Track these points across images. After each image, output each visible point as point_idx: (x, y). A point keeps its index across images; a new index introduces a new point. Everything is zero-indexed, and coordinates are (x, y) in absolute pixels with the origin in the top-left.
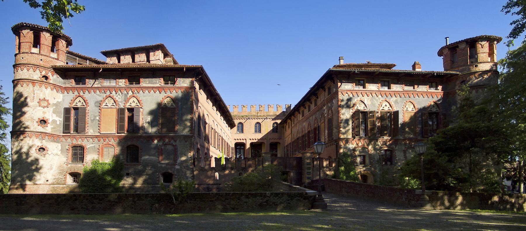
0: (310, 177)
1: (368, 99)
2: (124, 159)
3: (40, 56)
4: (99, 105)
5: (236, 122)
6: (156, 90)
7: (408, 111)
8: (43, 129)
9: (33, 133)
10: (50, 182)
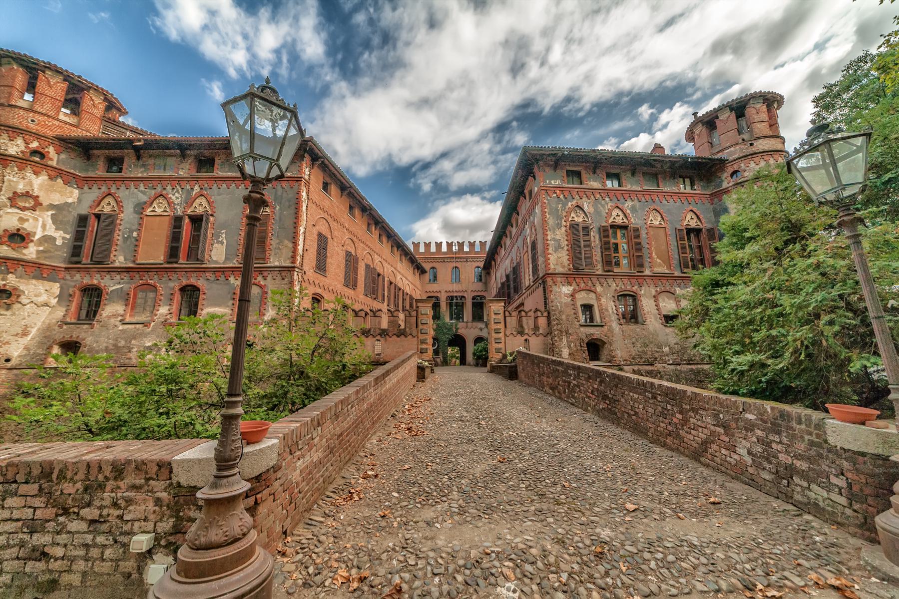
0: (501, 349)
3: (31, 115)
4: (141, 210)
5: (427, 266)
6: (240, 182)
7: (653, 225)
8: (14, 253)
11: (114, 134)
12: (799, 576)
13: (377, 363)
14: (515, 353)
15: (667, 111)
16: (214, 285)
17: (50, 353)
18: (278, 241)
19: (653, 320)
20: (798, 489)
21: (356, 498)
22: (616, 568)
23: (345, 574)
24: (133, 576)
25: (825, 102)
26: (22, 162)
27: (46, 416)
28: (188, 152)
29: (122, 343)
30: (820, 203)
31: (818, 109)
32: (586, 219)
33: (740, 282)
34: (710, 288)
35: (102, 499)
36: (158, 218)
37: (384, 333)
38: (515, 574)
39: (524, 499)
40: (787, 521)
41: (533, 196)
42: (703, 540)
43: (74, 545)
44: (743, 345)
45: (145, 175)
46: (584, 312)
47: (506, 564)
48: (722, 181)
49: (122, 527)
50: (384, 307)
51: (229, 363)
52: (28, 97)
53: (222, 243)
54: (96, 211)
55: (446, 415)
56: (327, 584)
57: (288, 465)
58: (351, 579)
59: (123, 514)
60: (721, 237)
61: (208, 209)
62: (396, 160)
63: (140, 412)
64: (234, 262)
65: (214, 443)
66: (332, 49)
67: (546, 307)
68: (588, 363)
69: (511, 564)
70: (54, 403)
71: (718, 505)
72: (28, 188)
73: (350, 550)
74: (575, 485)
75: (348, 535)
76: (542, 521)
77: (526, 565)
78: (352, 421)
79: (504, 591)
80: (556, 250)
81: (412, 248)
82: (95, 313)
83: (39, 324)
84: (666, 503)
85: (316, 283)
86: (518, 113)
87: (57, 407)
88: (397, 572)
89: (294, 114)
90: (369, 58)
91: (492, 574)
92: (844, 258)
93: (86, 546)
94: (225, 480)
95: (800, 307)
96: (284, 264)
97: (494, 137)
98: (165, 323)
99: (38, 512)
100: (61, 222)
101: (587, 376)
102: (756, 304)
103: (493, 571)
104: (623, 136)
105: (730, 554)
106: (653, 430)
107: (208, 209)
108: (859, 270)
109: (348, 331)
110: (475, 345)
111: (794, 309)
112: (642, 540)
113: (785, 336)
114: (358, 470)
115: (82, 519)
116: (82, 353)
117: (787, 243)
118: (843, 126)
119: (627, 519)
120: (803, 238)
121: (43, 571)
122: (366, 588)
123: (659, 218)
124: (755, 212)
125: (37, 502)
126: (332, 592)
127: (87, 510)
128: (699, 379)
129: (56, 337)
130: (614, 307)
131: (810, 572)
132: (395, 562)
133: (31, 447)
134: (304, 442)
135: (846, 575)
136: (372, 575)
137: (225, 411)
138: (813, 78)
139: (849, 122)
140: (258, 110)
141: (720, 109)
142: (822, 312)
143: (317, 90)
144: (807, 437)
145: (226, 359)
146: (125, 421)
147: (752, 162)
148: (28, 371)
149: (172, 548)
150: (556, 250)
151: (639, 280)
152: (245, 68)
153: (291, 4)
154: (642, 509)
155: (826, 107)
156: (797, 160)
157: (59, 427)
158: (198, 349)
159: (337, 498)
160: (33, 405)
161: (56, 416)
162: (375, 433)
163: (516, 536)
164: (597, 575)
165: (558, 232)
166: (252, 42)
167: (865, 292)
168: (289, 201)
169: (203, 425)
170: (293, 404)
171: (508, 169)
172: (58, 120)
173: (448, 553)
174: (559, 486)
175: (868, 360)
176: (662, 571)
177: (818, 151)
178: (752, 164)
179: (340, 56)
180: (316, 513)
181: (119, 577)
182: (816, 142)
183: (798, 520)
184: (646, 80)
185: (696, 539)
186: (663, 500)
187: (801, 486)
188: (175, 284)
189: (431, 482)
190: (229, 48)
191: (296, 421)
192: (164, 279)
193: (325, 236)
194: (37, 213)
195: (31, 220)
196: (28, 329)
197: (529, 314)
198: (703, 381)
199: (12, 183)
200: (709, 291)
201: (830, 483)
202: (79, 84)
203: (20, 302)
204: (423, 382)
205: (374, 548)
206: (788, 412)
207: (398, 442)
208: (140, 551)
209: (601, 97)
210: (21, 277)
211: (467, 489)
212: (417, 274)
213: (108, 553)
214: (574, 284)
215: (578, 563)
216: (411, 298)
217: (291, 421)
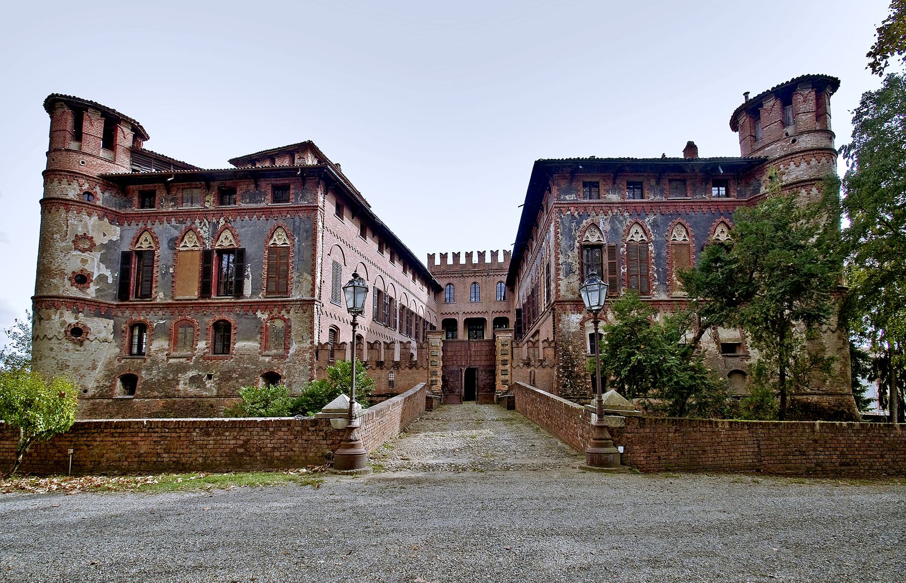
0: (507, 381)
1: (606, 220)
2: (207, 348)
5: (442, 283)
6: (261, 214)
9: (61, 300)
10: (90, 393)
32: (601, 239)
36: (190, 253)
48: (760, 185)
61: (233, 242)
80: (567, 275)
96: (305, 298)
123: (684, 233)
199: (74, 227)
202: (114, 117)
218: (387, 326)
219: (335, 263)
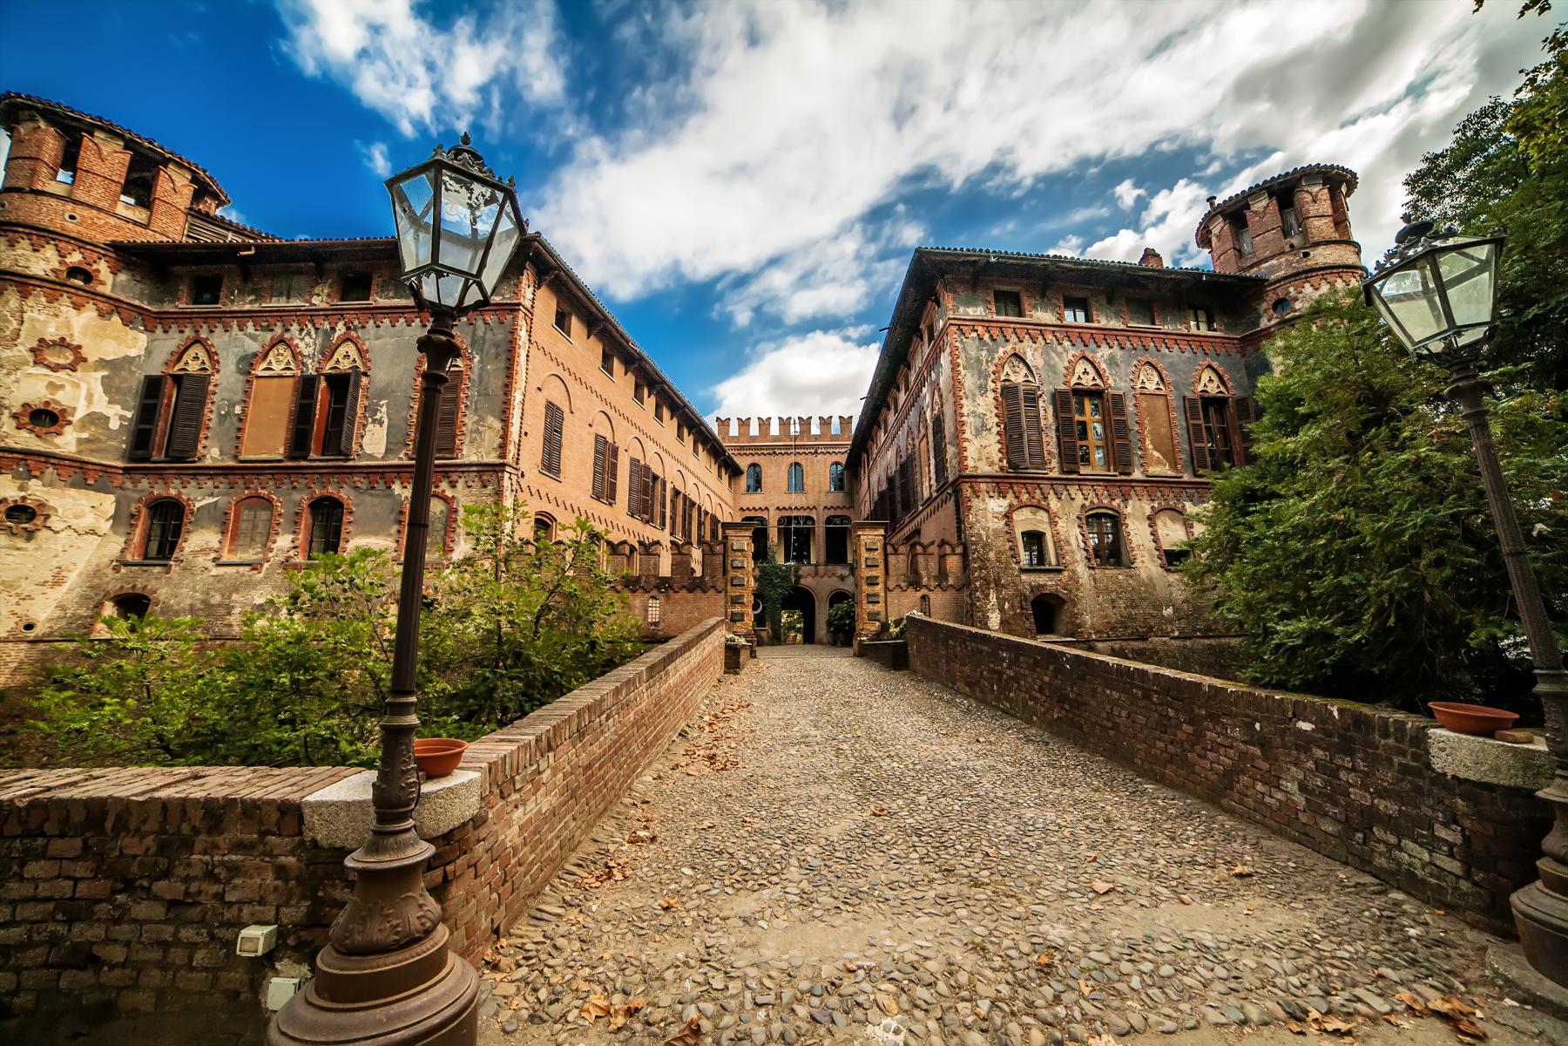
0: (878, 613)
3: (70, 206)
5: (743, 462)
6: (413, 316)
8: (41, 443)
11: (208, 236)
12: (1380, 995)
13: (653, 638)
14: (905, 622)
15: (1164, 192)
16: (368, 499)
17: (99, 614)
18: (476, 418)
19: (1146, 559)
20: (1382, 848)
21: (619, 876)
22: (1073, 989)
23: (603, 1003)
24: (243, 997)
25: (1426, 184)
26: (53, 287)
27: (93, 723)
28: (328, 266)
29: (217, 599)
30: (1420, 356)
31: (1415, 196)
32: (1030, 379)
33: (1291, 492)
34: (1242, 503)
35: (189, 865)
36: (276, 380)
37: (664, 585)
38: (898, 1003)
39: (916, 878)
40: (1361, 903)
41: (936, 334)
42: (1220, 937)
43: (143, 943)
44: (1292, 598)
45: (256, 307)
46: (1027, 547)
47: (885, 986)
48: (1260, 317)
49: (222, 914)
50: (665, 537)
51: (393, 636)
52: (63, 176)
53: (381, 423)
54: (175, 370)
55: (777, 733)
56: (570, 1017)
57: (499, 816)
58: (612, 1011)
59: (224, 891)
60: (1259, 414)
61: (359, 363)
62: (687, 270)
63: (247, 718)
64: (402, 455)
65: (372, 775)
66: (577, 83)
67: (959, 537)
68: (1034, 638)
69: (891, 987)
70: (107, 700)
71: (1248, 879)
72: (63, 333)
73: (610, 964)
74: (1007, 853)
75: (605, 938)
76: (947, 915)
77: (918, 988)
78: (609, 742)
79: (879, 1031)
80: (978, 433)
81: (714, 428)
82: (173, 546)
83: (81, 567)
84: (1161, 877)
85: (543, 494)
86: (907, 190)
87: (111, 706)
88: (692, 1002)
89: (510, 195)
90: (644, 97)
91: (859, 1005)
92: (1459, 453)
93: (164, 945)
94: (391, 840)
95: (1388, 536)
96: (486, 460)
97: (864, 231)
98: (286, 565)
99: (82, 886)
100: (118, 390)
101: (1031, 661)
102: (1316, 530)
103: (861, 999)
104: (1091, 233)
105: (1265, 960)
106: (1143, 753)
107: (359, 363)
108: (1484, 473)
109: (599, 581)
110: (831, 606)
111: (1379, 539)
112: (1118, 942)
113: (1364, 586)
114: (620, 828)
115: (156, 898)
116: (151, 614)
117: (1367, 425)
118: (1456, 225)
119: (1095, 906)
120: (1393, 417)
121: (90, 986)
122: (638, 1027)
123: (1156, 379)
124: (1314, 370)
125: (80, 870)
126: (579, 1031)
127: (163, 884)
128: (1221, 664)
129: (110, 587)
130: (1080, 537)
131: (1399, 988)
132: (688, 984)
133: (69, 775)
134: (523, 779)
135: (1461, 994)
136: (649, 1004)
137: (386, 720)
138: (1404, 142)
139: (1466, 218)
140: (447, 190)
141: (1254, 192)
142: (1425, 545)
143: (551, 153)
144: (1396, 760)
145: (387, 630)
146: (224, 734)
147: (1307, 285)
148: (64, 645)
149: (306, 953)
150: (978, 433)
151: (1124, 489)
152: (428, 120)
153: (509, 12)
154: (1121, 890)
155: (1428, 194)
156: (1381, 282)
157: (116, 742)
158: (341, 611)
159: (585, 875)
160: (71, 703)
161: (110, 722)
162: (650, 764)
163: (901, 941)
164: (1039, 1002)
165: (980, 400)
166: (442, 75)
167: (1494, 510)
168: (497, 346)
169: (351, 743)
170: (505, 710)
171: (891, 286)
172: (115, 215)
173: (783, 971)
174: (979, 855)
175: (1500, 626)
176: (1150, 992)
177: (1415, 268)
178: (1308, 289)
179: (591, 95)
180: (548, 899)
181: (218, 998)
182: (1411, 253)
183: (1380, 901)
184: (1129, 141)
185: (1210, 937)
186: (1155, 874)
187: (1386, 843)
188: (303, 496)
189: (751, 851)
190: (402, 86)
191: (510, 741)
192: (284, 487)
193: (558, 408)
194: (78, 374)
195: (68, 387)
196: (63, 574)
197: (930, 549)
198: (1229, 667)
199: (36, 324)
200: (1241, 509)
201: (1434, 836)
202: (151, 154)
203: (49, 528)
204: (737, 673)
205: (651, 961)
206: (1366, 716)
207: (691, 780)
208: (253, 955)
209: (1051, 167)
210: (51, 485)
211: (815, 862)
212: (725, 477)
213: (200, 957)
214: (1010, 495)
215: (1008, 983)
216: (714, 520)
217: (502, 740)
218: (647, 522)
219: (551, 407)
